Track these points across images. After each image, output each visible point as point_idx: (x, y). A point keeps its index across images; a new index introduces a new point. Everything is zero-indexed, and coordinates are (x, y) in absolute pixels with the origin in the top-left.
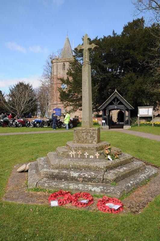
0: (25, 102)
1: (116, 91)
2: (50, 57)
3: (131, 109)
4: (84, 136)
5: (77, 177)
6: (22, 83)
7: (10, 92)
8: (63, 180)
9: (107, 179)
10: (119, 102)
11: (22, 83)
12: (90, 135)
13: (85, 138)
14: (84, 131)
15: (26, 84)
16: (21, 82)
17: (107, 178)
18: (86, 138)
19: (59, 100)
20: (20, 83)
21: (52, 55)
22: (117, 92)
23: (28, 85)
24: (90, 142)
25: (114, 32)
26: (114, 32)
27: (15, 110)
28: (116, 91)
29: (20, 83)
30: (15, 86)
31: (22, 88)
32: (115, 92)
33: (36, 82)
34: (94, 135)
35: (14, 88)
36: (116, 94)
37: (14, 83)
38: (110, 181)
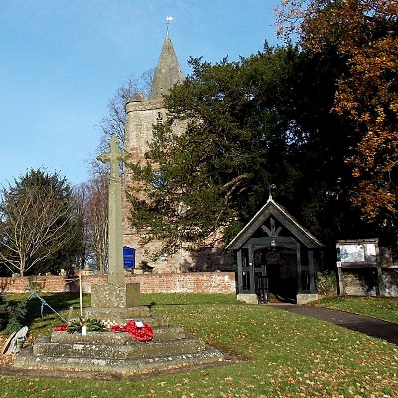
0: (42, 229)
1: (270, 199)
2: (122, 93)
3: (313, 246)
4: (107, 296)
5: (82, 350)
6: (39, 172)
7: (4, 197)
8: (63, 355)
9: (120, 352)
10: (280, 228)
11: (39, 172)
12: (115, 293)
13: (108, 299)
14: (106, 288)
15: (51, 175)
16: (36, 170)
17: (120, 350)
18: (110, 299)
19: (127, 223)
20: (33, 171)
21: (127, 87)
22: (273, 201)
23: (55, 177)
24: (115, 306)
25: (266, 44)
26: (266, 44)
27: (51, 229)
28: (270, 199)
29: (33, 171)
30: (19, 181)
31: (40, 187)
32: (268, 202)
33: (76, 174)
34: (121, 295)
35: (14, 186)
36: (271, 207)
37: (21, 171)
38: (124, 354)
